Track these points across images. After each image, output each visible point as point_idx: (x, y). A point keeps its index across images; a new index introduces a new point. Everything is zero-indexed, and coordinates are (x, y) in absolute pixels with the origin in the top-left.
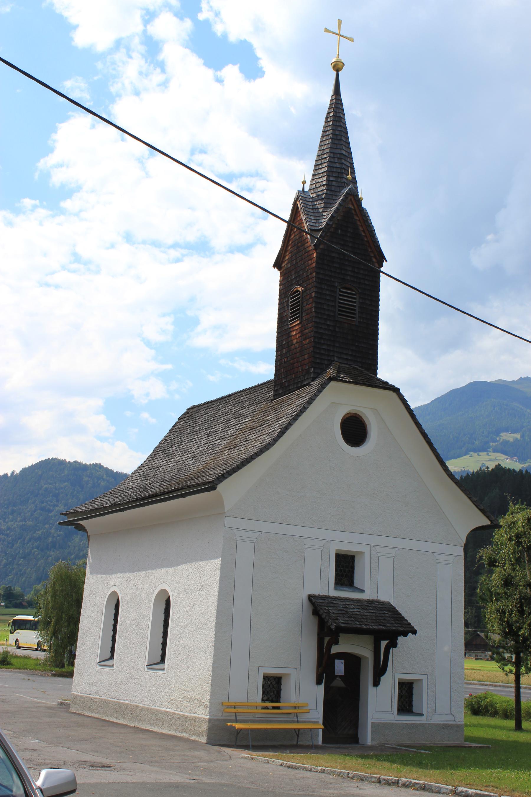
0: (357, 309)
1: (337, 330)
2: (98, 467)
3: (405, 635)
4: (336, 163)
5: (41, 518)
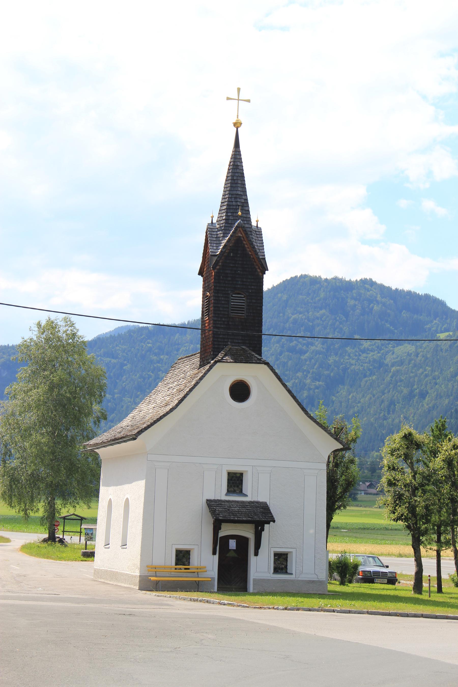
1: (230, 323)
2: (368, 284)
3: (268, 523)
4: (232, 202)
5: (290, 363)
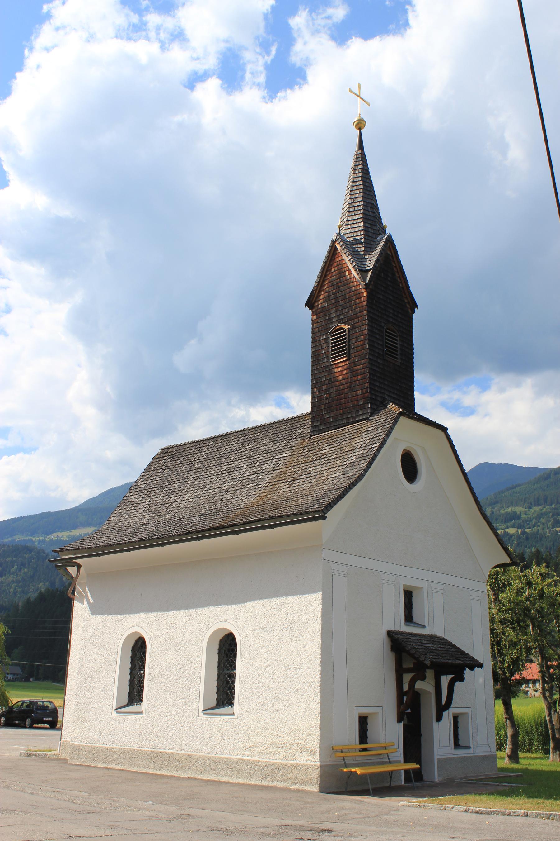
0: (399, 349)
3: (472, 668)
4: (369, 211)
